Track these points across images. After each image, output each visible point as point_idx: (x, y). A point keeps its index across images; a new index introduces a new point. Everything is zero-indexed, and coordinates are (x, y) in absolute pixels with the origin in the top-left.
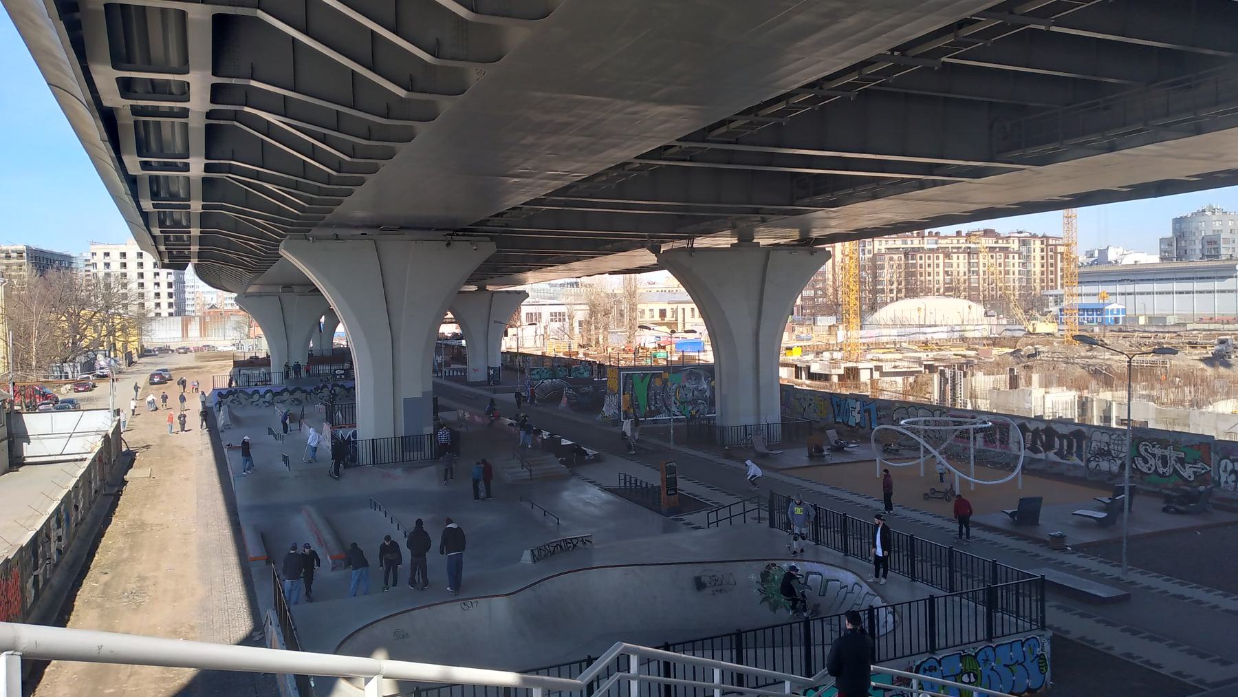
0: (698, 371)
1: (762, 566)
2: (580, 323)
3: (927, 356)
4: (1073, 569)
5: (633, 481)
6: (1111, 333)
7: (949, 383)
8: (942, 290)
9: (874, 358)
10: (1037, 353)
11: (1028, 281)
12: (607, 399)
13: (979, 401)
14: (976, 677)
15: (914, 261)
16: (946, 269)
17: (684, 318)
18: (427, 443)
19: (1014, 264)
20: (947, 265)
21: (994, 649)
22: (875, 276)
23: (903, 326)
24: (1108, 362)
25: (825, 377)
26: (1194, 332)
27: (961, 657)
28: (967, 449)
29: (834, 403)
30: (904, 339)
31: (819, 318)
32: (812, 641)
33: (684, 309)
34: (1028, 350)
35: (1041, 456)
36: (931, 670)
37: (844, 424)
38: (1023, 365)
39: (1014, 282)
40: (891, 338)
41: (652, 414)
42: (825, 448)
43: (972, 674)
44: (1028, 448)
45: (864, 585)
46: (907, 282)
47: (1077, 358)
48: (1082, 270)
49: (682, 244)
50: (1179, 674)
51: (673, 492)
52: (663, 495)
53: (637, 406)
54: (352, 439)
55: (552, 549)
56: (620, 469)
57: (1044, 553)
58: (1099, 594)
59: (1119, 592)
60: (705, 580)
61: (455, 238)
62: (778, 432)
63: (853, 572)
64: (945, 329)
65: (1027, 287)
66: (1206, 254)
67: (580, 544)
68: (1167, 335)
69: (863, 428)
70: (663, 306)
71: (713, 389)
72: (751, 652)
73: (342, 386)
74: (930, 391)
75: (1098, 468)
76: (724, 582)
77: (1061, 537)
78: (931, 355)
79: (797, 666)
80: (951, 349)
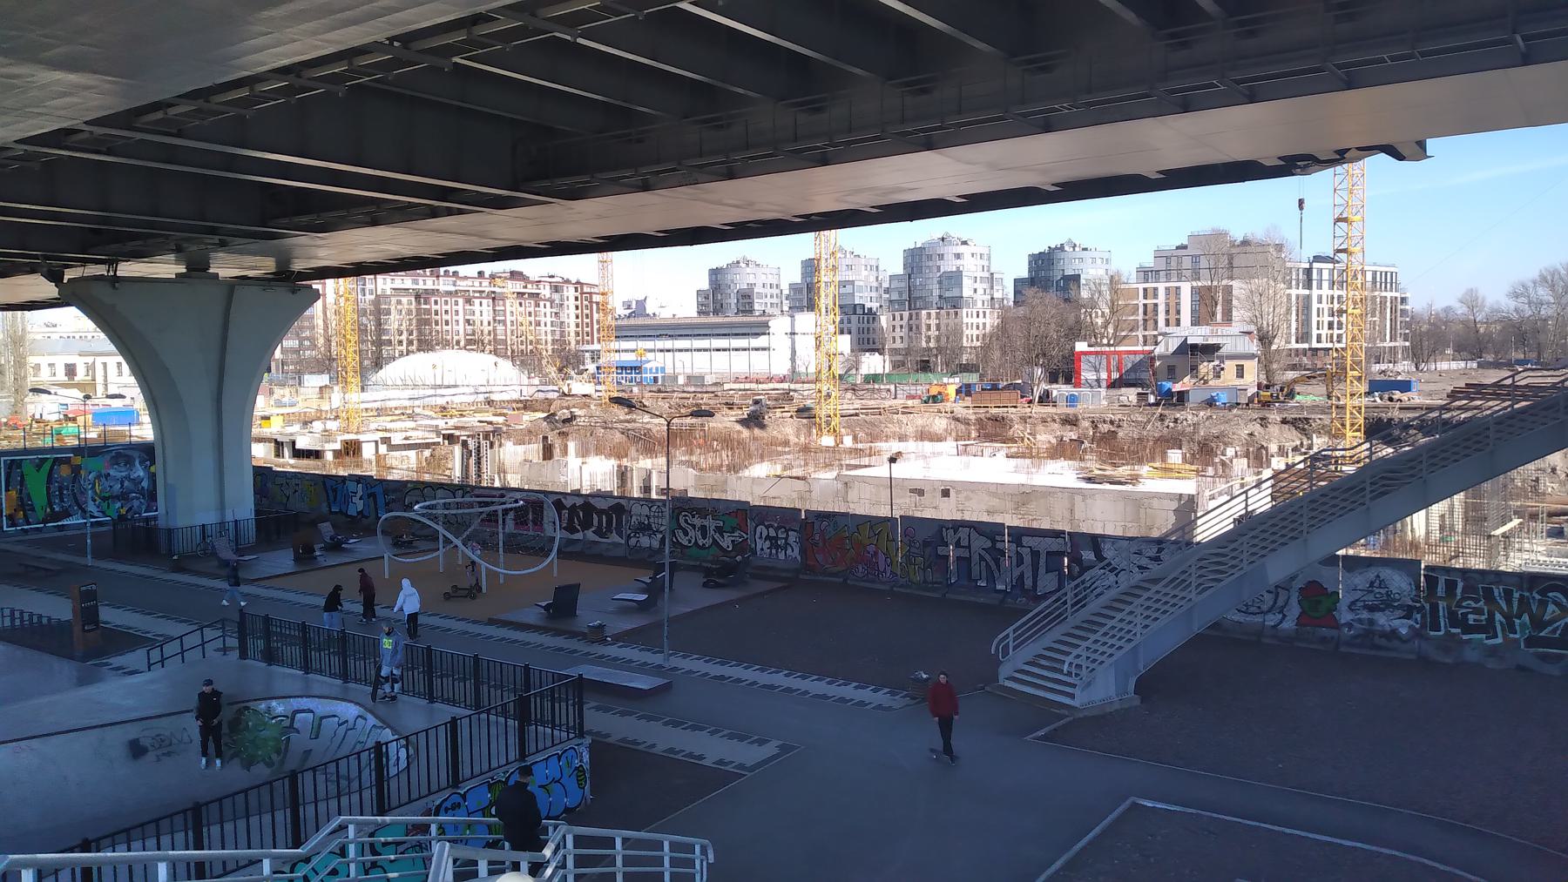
0: (129, 453)
3: (446, 423)
4: (614, 662)
5: (26, 617)
7: (473, 456)
8: (462, 344)
9: (380, 428)
11: (562, 334)
15: (428, 307)
16: (467, 317)
17: (106, 377)
20: (468, 312)
22: (379, 324)
23: (415, 386)
24: (648, 426)
26: (731, 392)
30: (417, 403)
31: (306, 377)
33: (105, 364)
34: (564, 414)
35: (579, 536)
38: (558, 431)
39: (546, 335)
45: (369, 716)
46: (420, 333)
47: (615, 422)
49: (101, 270)
52: (77, 629)
59: (659, 681)
60: (146, 742)
65: (561, 342)
69: (367, 517)
70: (70, 360)
72: (215, 829)
74: (450, 466)
75: (638, 545)
77: (601, 627)
78: (452, 422)
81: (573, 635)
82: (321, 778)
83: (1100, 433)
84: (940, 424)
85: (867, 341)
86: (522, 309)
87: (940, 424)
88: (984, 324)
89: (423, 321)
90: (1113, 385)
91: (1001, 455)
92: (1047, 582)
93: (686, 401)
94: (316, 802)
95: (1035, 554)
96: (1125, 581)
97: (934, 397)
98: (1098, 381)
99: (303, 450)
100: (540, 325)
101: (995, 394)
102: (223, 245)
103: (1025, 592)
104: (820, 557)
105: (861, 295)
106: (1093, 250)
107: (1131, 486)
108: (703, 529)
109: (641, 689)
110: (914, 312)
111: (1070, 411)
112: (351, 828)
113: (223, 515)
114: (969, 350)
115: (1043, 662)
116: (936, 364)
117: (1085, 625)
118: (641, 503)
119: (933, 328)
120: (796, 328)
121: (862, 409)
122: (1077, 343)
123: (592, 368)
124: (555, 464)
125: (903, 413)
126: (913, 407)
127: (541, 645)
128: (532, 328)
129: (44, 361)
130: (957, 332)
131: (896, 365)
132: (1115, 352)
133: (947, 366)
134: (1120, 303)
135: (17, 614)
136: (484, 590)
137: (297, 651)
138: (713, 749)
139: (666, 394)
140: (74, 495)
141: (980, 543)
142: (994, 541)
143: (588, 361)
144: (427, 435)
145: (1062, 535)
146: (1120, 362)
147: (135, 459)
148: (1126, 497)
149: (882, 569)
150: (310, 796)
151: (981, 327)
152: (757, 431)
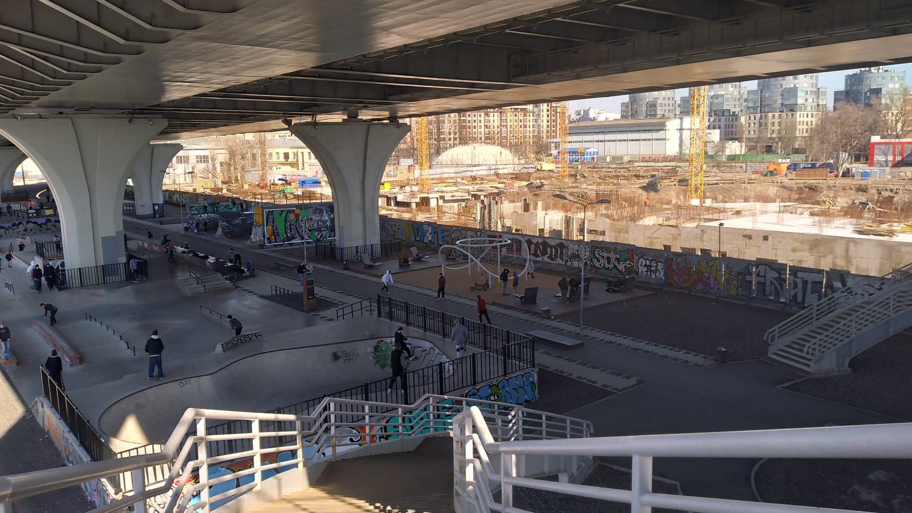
0: (320, 207)
1: (374, 343)
2: (221, 164)
3: (474, 188)
4: (554, 330)
5: (282, 290)
6: (588, 169)
7: (487, 209)
8: (483, 139)
9: (439, 190)
10: (542, 185)
11: (539, 132)
12: (254, 230)
13: (505, 220)
14: (498, 396)
15: (465, 118)
16: (486, 124)
17: (303, 160)
18: (122, 269)
19: (529, 120)
20: (487, 121)
21: (507, 380)
22: (439, 129)
23: (458, 165)
24: (585, 191)
25: (407, 205)
26: (638, 168)
27: (490, 386)
28: (496, 256)
29: (415, 228)
30: (458, 175)
31: (401, 160)
32: (408, 385)
33: (303, 153)
34: (537, 183)
35: (540, 259)
36: (474, 395)
37: (421, 241)
38: (533, 193)
39: (530, 133)
40: (451, 174)
41: (288, 239)
42: (409, 259)
43: (496, 395)
44: (532, 254)
45: (436, 348)
46: (460, 132)
47: (566, 188)
48: (573, 125)
49: (309, 119)
50: (605, 386)
51: (312, 297)
52: (305, 297)
53: (277, 234)
54: (60, 268)
55: (235, 342)
56: (270, 282)
57: (538, 320)
58: (566, 344)
59: (578, 342)
60: (339, 354)
61: (135, 116)
62: (378, 249)
63: (429, 342)
64: (484, 168)
65: (538, 137)
66: (649, 113)
67: (254, 338)
68: (622, 170)
69: (433, 244)
70: (286, 150)
71: (333, 220)
72: (373, 395)
73: (35, 223)
74: (475, 212)
75: (572, 265)
76: (351, 354)
77: (548, 311)
78: (476, 187)
79: (399, 400)
80: (489, 183)
81: (534, 314)
82: (416, 376)
83: (882, 197)
84: (772, 190)
85: (730, 135)
86: (517, 118)
87: (772, 190)
88: (812, 122)
89: (462, 127)
90: (896, 165)
91: (807, 214)
92: (811, 299)
93: (610, 174)
94: (424, 384)
95: (805, 282)
96: (859, 301)
97: (771, 172)
98: (886, 161)
99: (401, 202)
100: (526, 128)
101: (812, 171)
102: (365, 107)
103: (797, 304)
104: (675, 278)
105: (728, 103)
106: (892, 71)
107: (888, 237)
108: (609, 259)
109: (567, 345)
110: (763, 114)
111: (863, 182)
112: (431, 399)
113: (365, 242)
114: (800, 139)
115: (796, 346)
116: (777, 148)
117: (824, 327)
118: (574, 243)
119: (776, 124)
120: (683, 126)
121: (721, 180)
122: (872, 137)
123: (554, 152)
124: (531, 214)
125: (748, 183)
126: (756, 179)
127: (518, 318)
128: (522, 129)
129: (273, 151)
130: (793, 127)
131: (750, 149)
132: (899, 143)
133: (784, 149)
134: (907, 108)
135: (278, 289)
136: (490, 287)
137: (403, 314)
138: (600, 378)
139: (598, 169)
140: (297, 228)
141: (772, 275)
142: (780, 274)
143: (553, 148)
144: (463, 194)
145: (822, 272)
146: (903, 149)
147: (323, 211)
148: (881, 243)
149: (712, 286)
150: (412, 384)
151: (809, 123)
152: (652, 194)
